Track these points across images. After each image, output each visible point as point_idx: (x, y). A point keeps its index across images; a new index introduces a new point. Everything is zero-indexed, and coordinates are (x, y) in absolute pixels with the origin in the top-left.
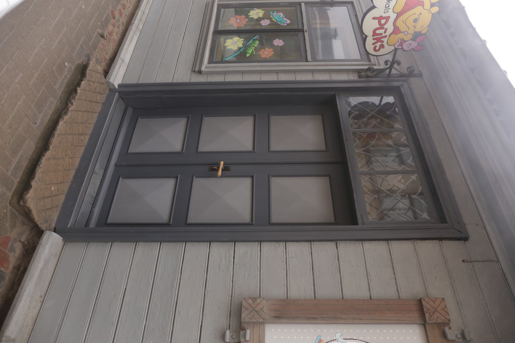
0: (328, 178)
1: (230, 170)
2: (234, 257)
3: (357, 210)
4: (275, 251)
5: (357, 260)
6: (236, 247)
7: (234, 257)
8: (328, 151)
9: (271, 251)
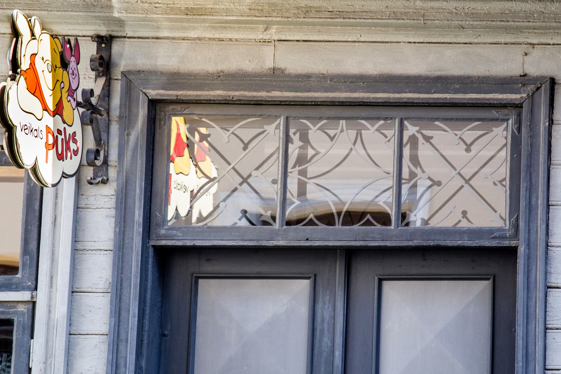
8: (315, 275)
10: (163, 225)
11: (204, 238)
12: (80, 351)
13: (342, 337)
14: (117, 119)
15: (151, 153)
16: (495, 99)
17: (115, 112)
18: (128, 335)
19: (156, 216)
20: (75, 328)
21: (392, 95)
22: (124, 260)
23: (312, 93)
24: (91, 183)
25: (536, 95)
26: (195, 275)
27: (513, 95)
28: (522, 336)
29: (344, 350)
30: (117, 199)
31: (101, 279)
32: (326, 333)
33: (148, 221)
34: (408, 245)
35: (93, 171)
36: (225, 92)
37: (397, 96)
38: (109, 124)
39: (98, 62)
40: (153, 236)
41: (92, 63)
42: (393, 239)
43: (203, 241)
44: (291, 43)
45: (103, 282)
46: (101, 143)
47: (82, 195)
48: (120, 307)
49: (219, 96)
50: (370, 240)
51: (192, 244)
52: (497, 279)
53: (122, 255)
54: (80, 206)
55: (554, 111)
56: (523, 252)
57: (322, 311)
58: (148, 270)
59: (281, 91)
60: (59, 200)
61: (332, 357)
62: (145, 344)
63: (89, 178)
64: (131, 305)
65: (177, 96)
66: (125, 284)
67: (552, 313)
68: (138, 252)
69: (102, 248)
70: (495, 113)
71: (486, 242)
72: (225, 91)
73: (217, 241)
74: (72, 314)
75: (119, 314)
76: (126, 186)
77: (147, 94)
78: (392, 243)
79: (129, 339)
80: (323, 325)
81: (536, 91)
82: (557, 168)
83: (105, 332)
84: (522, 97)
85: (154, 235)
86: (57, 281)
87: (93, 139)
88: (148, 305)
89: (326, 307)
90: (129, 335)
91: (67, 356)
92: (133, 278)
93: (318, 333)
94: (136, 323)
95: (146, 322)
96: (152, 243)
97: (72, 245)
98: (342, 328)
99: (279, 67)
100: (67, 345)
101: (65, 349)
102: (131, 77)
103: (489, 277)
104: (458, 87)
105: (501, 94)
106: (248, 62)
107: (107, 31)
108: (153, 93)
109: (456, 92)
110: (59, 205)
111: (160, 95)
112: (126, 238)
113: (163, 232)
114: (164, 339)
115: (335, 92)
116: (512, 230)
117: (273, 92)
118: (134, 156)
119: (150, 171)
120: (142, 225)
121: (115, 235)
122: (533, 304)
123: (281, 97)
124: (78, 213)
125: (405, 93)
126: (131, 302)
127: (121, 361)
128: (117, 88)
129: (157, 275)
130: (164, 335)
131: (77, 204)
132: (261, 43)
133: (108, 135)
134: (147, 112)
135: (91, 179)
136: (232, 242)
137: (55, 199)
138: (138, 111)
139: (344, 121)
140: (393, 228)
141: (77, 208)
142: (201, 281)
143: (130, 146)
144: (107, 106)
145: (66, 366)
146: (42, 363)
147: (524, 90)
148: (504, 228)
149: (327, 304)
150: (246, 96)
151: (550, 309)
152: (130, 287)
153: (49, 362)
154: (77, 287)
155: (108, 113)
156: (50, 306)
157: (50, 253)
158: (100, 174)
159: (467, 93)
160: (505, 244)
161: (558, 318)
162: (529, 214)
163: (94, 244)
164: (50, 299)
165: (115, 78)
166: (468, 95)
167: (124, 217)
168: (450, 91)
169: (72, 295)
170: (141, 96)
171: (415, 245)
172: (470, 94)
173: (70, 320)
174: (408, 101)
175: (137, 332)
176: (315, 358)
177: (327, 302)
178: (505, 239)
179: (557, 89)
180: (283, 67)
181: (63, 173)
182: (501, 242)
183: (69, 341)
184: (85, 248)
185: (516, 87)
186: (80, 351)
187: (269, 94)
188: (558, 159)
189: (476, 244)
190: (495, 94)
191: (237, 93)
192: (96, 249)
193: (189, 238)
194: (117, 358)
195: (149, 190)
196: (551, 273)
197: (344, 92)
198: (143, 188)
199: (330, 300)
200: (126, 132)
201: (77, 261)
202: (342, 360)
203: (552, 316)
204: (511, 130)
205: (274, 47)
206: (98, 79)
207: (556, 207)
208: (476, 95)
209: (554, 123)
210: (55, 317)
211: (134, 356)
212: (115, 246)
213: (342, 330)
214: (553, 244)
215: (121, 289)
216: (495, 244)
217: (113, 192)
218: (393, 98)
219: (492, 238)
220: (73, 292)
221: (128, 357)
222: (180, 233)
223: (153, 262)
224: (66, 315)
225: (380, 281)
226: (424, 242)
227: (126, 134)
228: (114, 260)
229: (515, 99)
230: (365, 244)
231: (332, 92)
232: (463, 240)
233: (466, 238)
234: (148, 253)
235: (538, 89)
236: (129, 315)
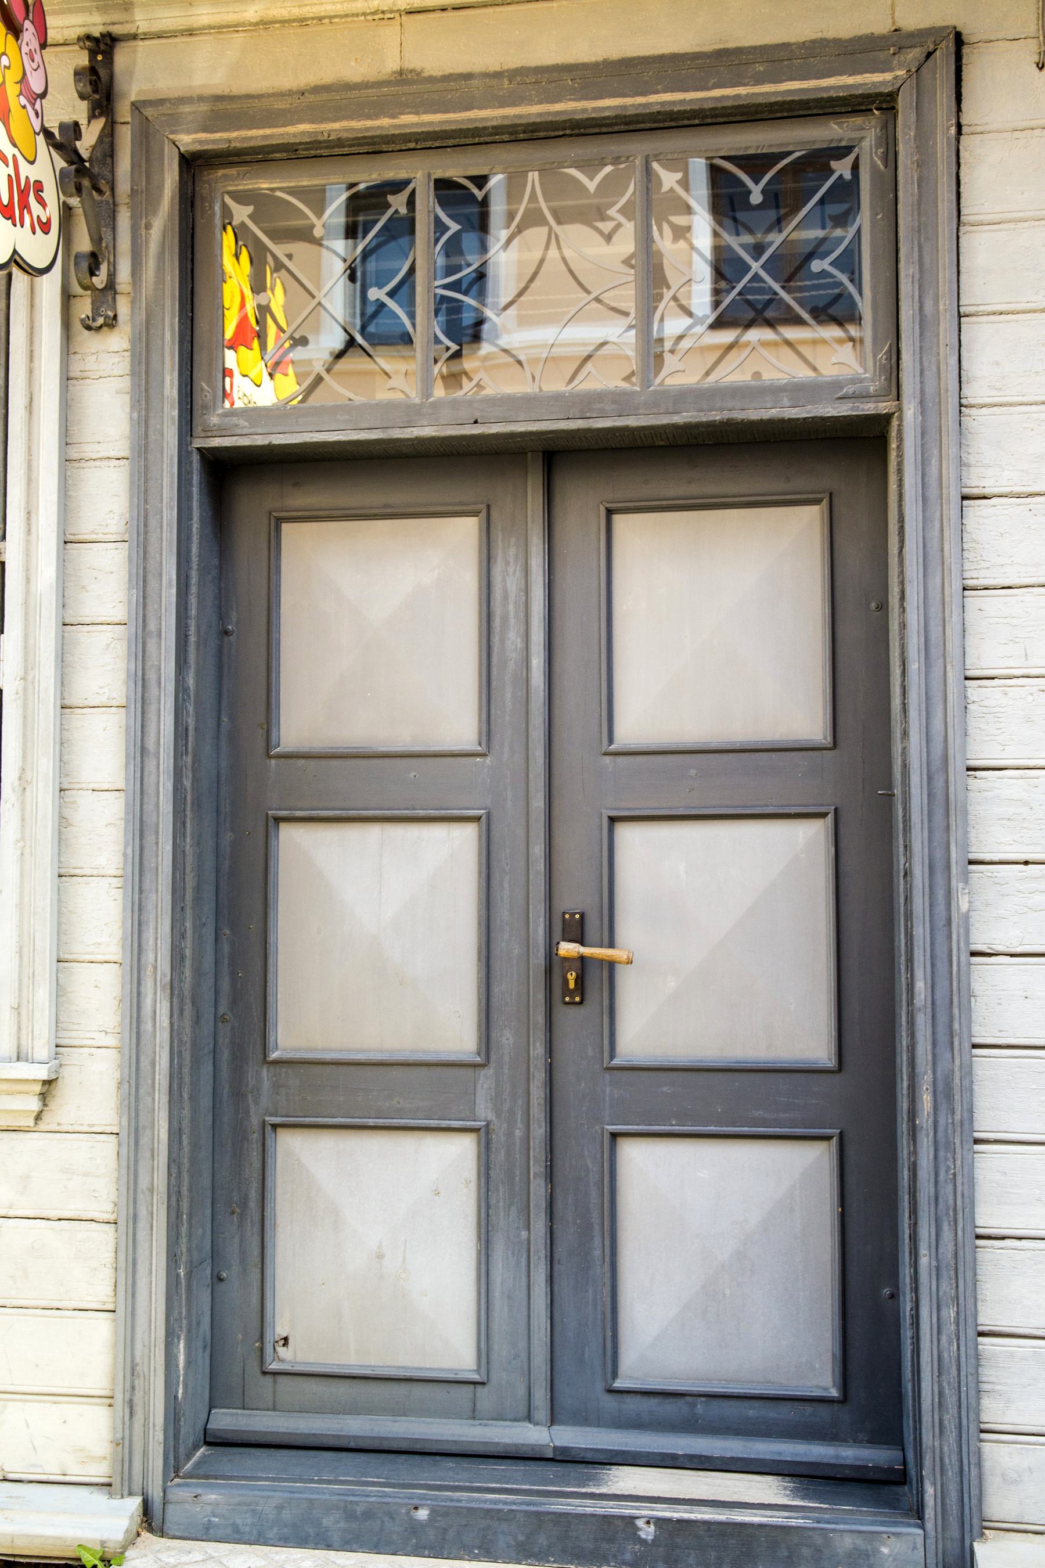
0: (620, 521)
1: (582, 915)
2: (1026, 863)
3: (819, 414)
4: (1000, 715)
5: (1032, 430)
6: (987, 857)
7: (1026, 863)
8: (489, 507)
9: (1000, 731)
10: (214, 406)
11: (286, 429)
12: (81, 657)
13: (542, 629)
14: (128, 201)
15: (189, 267)
16: (840, 87)
17: (124, 186)
18: (160, 624)
19: (202, 390)
20: (71, 611)
21: (629, 101)
22: (149, 475)
23: (476, 111)
24: (89, 328)
25: (924, 70)
26: (275, 514)
27: (876, 75)
28: (916, 604)
29: (547, 654)
30: (132, 356)
31: (112, 516)
32: (512, 621)
33: (189, 400)
34: (671, 422)
35: (90, 306)
36: (313, 126)
37: (640, 100)
38: (114, 211)
39: (88, 79)
40: (198, 430)
41: (78, 77)
42: (641, 411)
43: (287, 435)
44: (431, 15)
45: (116, 522)
46: (101, 246)
47: (75, 353)
48: (145, 568)
49: (303, 133)
50: (595, 416)
51: (266, 442)
52: (835, 501)
53: (146, 466)
54: (72, 374)
55: (962, 106)
56: (912, 419)
57: (504, 580)
58: (192, 498)
59: (417, 113)
60: (36, 364)
61: (525, 670)
62: (192, 644)
63: (83, 316)
64: (164, 563)
65: (230, 141)
66: (153, 522)
67: (975, 555)
68: (172, 457)
69: (112, 454)
70: (836, 127)
71: (827, 407)
72: (313, 123)
73: (311, 435)
74: (66, 584)
75: (145, 581)
76: (147, 328)
77: (177, 143)
78: (639, 419)
79: (163, 630)
80: (507, 608)
81: (925, 61)
82: (973, 232)
83: (122, 618)
84: (896, 78)
85: (200, 428)
86: (38, 519)
87: (89, 238)
88: (194, 566)
89: (511, 570)
90: (163, 623)
91: (60, 666)
92: (164, 510)
93: (497, 622)
94: (174, 599)
95: (193, 601)
96: (198, 443)
97: (60, 452)
98: (542, 611)
99: (411, 67)
100: (60, 647)
101: (56, 651)
102: (149, 112)
103: (818, 496)
104: (762, 69)
105: (850, 75)
106: (353, 63)
107: (104, 24)
108: (188, 140)
109: (759, 81)
110: (36, 372)
111: (199, 142)
112: (151, 432)
113: (214, 420)
114: (226, 639)
115: (519, 105)
116: (880, 378)
117: (402, 117)
118: (160, 270)
119: (189, 302)
120: (177, 405)
121: (132, 426)
122: (937, 533)
123: (417, 124)
124: (69, 388)
125: (656, 93)
126: (164, 557)
127: (152, 676)
128: (125, 136)
129: (210, 514)
130: (226, 633)
131: (68, 371)
132: (376, 23)
133: (114, 235)
134: (177, 178)
135: (88, 317)
136: (338, 435)
137: (28, 362)
138: (163, 177)
139: (537, 173)
140: (638, 389)
141: (67, 379)
142: (285, 527)
143: (151, 250)
144: (111, 176)
145: (59, 684)
146: (18, 678)
147: (899, 61)
148: (863, 376)
149: (511, 563)
150: (353, 130)
151: (970, 545)
152: (161, 527)
153: (30, 678)
154: (73, 532)
155: (113, 190)
156: (28, 570)
157: (24, 466)
158: (401, 1101)
159: (781, 82)
160: (868, 410)
161: (988, 565)
162: (921, 335)
163: (98, 447)
164: (27, 555)
165: (123, 121)
166: (784, 84)
167: (146, 390)
168: (746, 81)
169: (65, 549)
170: (168, 148)
171: (685, 423)
172: (789, 83)
173: (64, 596)
174: (663, 109)
175: (177, 617)
176: (494, 672)
177: (512, 560)
178: (868, 400)
179: (967, 54)
180: (418, 68)
181: (15, 252)
182: (858, 407)
183: (63, 637)
184: (83, 455)
185: (882, 55)
186: (81, 657)
187: (396, 121)
188: (975, 212)
189: (808, 412)
190: (839, 78)
191: (336, 126)
192: (101, 456)
193: (260, 431)
194: (143, 669)
195: (189, 338)
196: (969, 466)
197: (536, 104)
198: (177, 329)
199: (517, 555)
200: (144, 221)
201: (70, 482)
202: (545, 675)
203: (975, 560)
204: (868, 161)
205: (399, 27)
206: (93, 122)
207: (974, 319)
208: (799, 82)
209: (963, 132)
210: (37, 590)
211: (173, 664)
212: (132, 449)
213: (542, 614)
214: (972, 401)
215: (146, 533)
216: (847, 411)
217: (126, 345)
218: (633, 105)
219: (839, 398)
220: (65, 542)
221: (163, 666)
222: (245, 421)
223: (201, 483)
224: (54, 584)
225: (610, 512)
226: (702, 414)
227: (143, 226)
228: (132, 475)
229: (883, 83)
230: (586, 426)
231: (514, 104)
232: (779, 406)
233: (786, 402)
234: (191, 462)
235: (929, 55)
236: (161, 585)
